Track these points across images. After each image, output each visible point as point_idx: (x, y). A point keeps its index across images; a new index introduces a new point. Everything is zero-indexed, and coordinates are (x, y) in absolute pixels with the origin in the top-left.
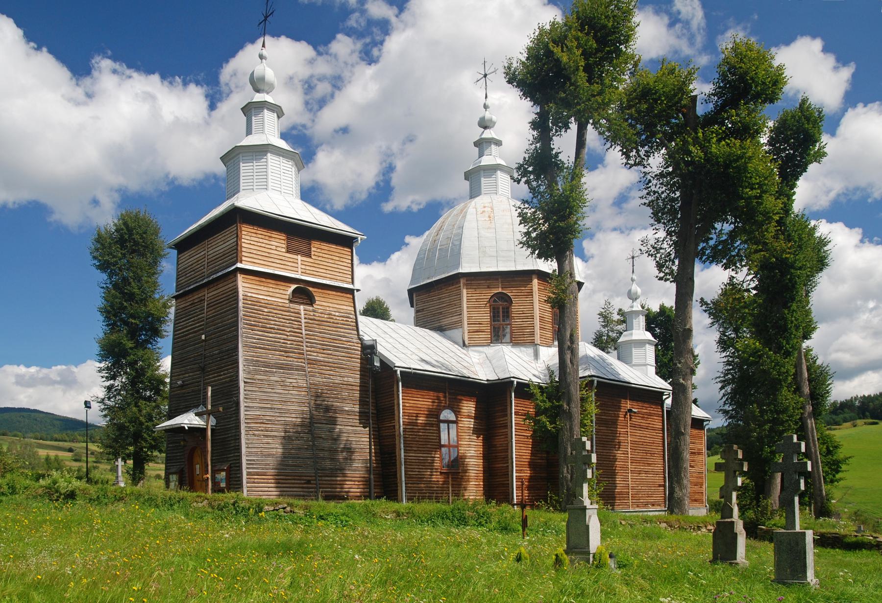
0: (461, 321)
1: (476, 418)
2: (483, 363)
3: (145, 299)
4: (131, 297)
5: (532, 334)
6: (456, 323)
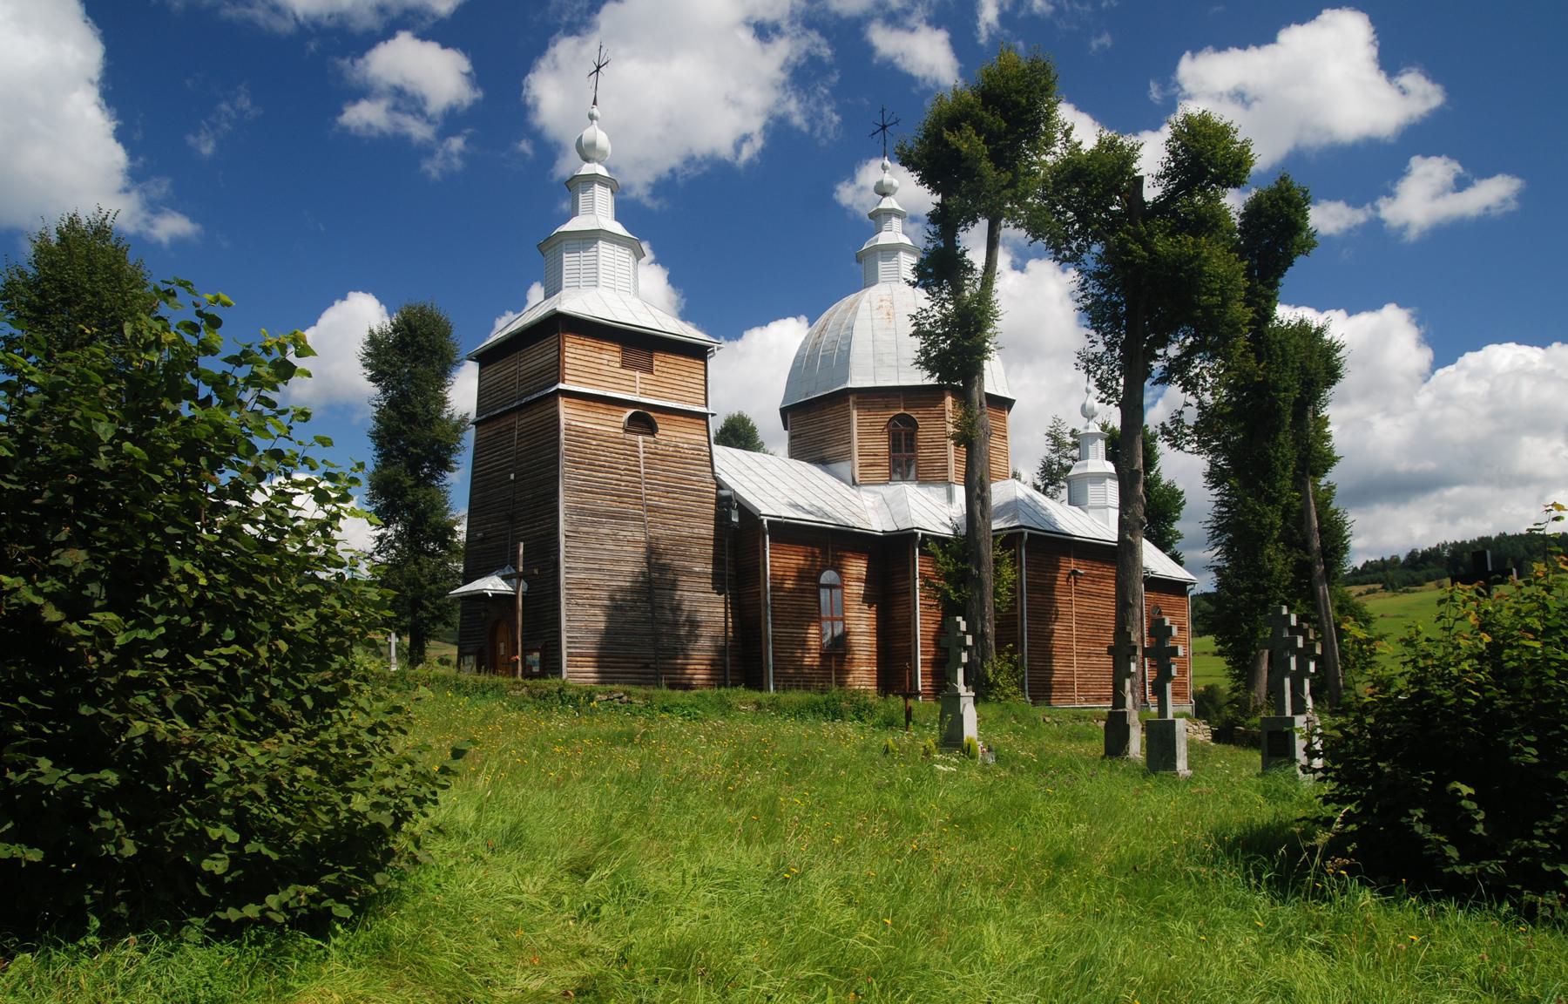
0: (850, 452)
1: (866, 581)
2: (875, 507)
3: (431, 421)
4: (412, 418)
5: (945, 469)
6: (843, 453)
